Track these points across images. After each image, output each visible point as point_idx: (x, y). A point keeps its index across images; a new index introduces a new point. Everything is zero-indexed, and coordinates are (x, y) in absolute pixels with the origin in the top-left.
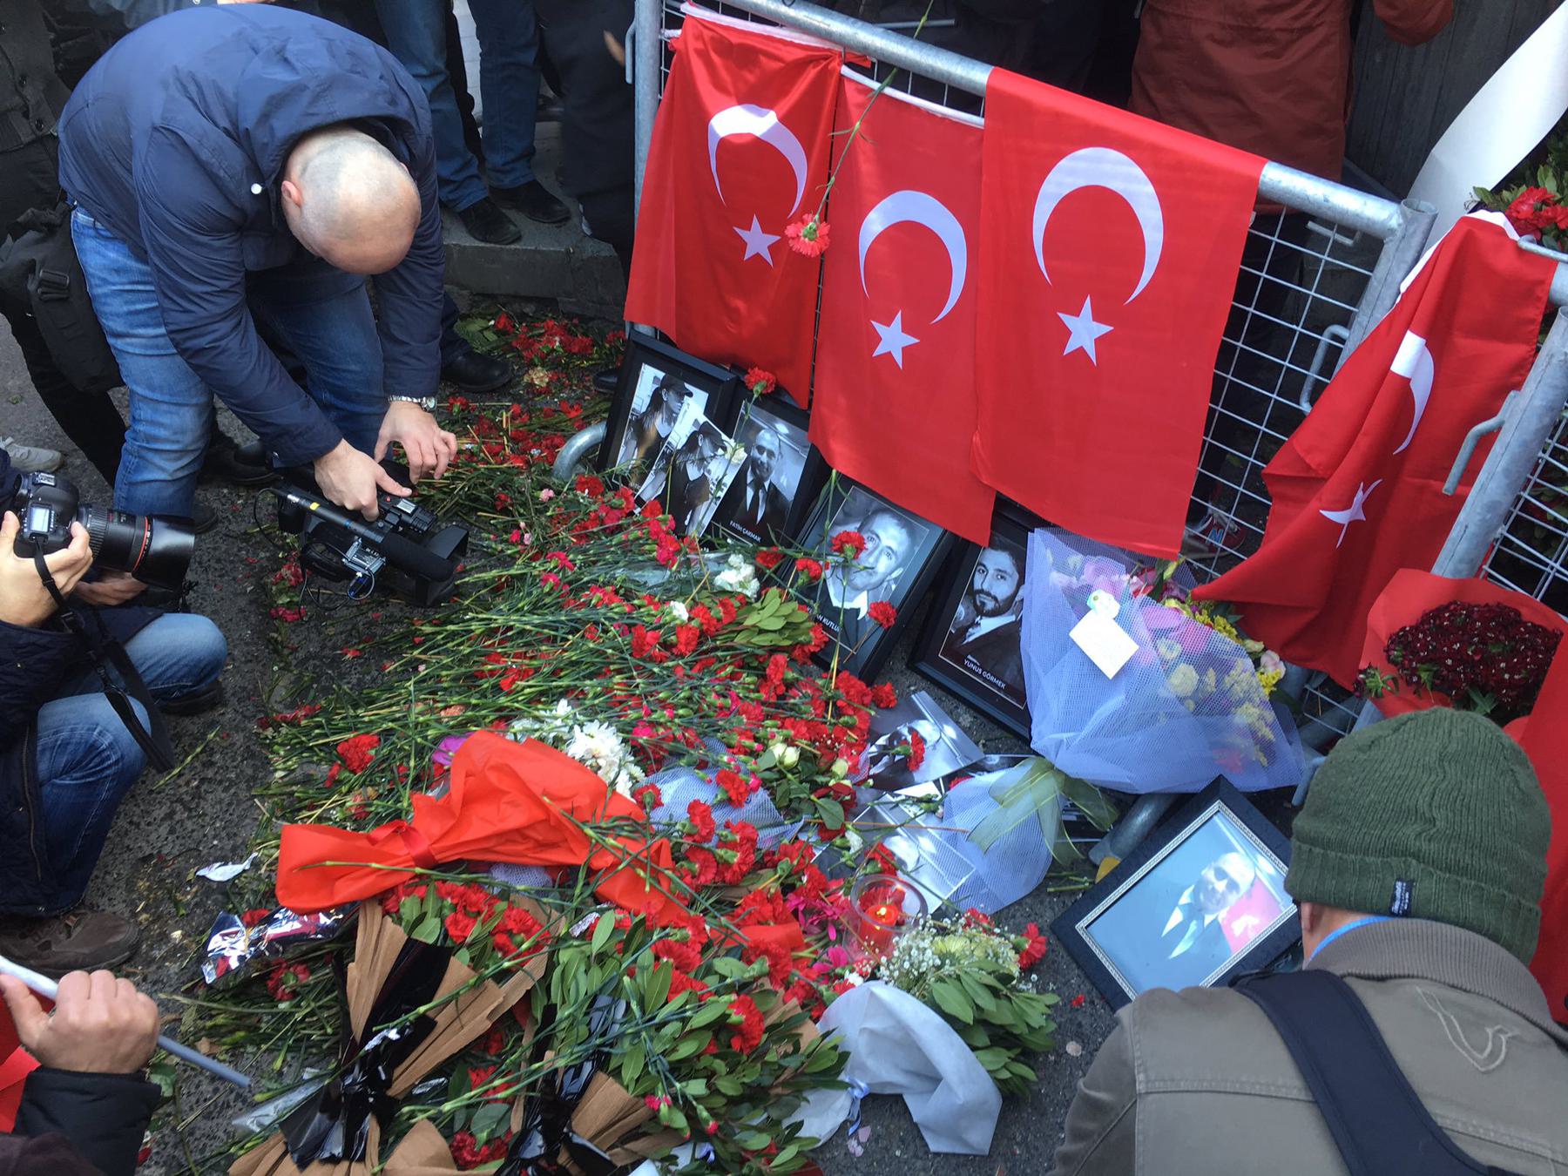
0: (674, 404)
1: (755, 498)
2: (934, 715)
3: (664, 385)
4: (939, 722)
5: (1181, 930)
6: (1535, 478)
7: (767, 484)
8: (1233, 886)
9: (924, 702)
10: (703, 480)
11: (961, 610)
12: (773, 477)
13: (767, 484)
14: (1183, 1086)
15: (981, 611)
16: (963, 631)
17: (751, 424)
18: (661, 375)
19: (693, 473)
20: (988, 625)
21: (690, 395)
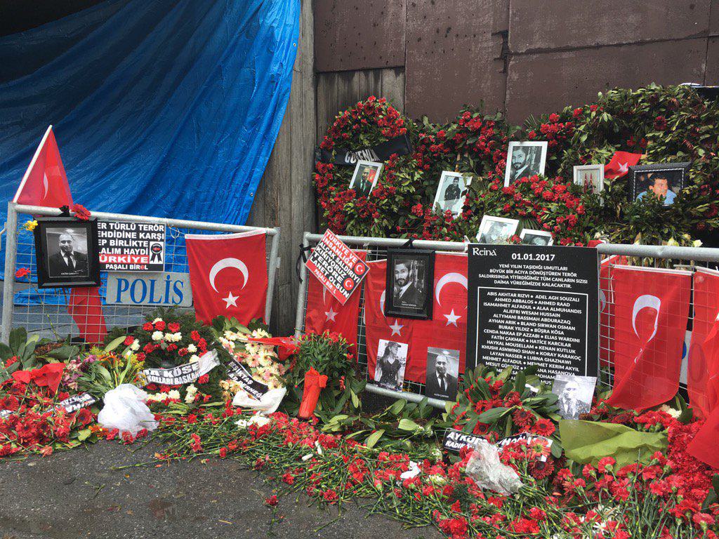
0: (394, 352)
1: (442, 381)
2: (438, 352)
3: (390, 345)
4: (441, 352)
5: (70, 261)
6: (164, 271)
7: (445, 375)
8: (367, 173)
9: (432, 350)
10: (397, 361)
11: (395, 288)
12: (447, 372)
13: (445, 375)
14: (289, 172)
15: (402, 285)
16: (398, 294)
17: (431, 355)
18: (387, 342)
19: (391, 361)
20: (405, 289)
21: (400, 346)
